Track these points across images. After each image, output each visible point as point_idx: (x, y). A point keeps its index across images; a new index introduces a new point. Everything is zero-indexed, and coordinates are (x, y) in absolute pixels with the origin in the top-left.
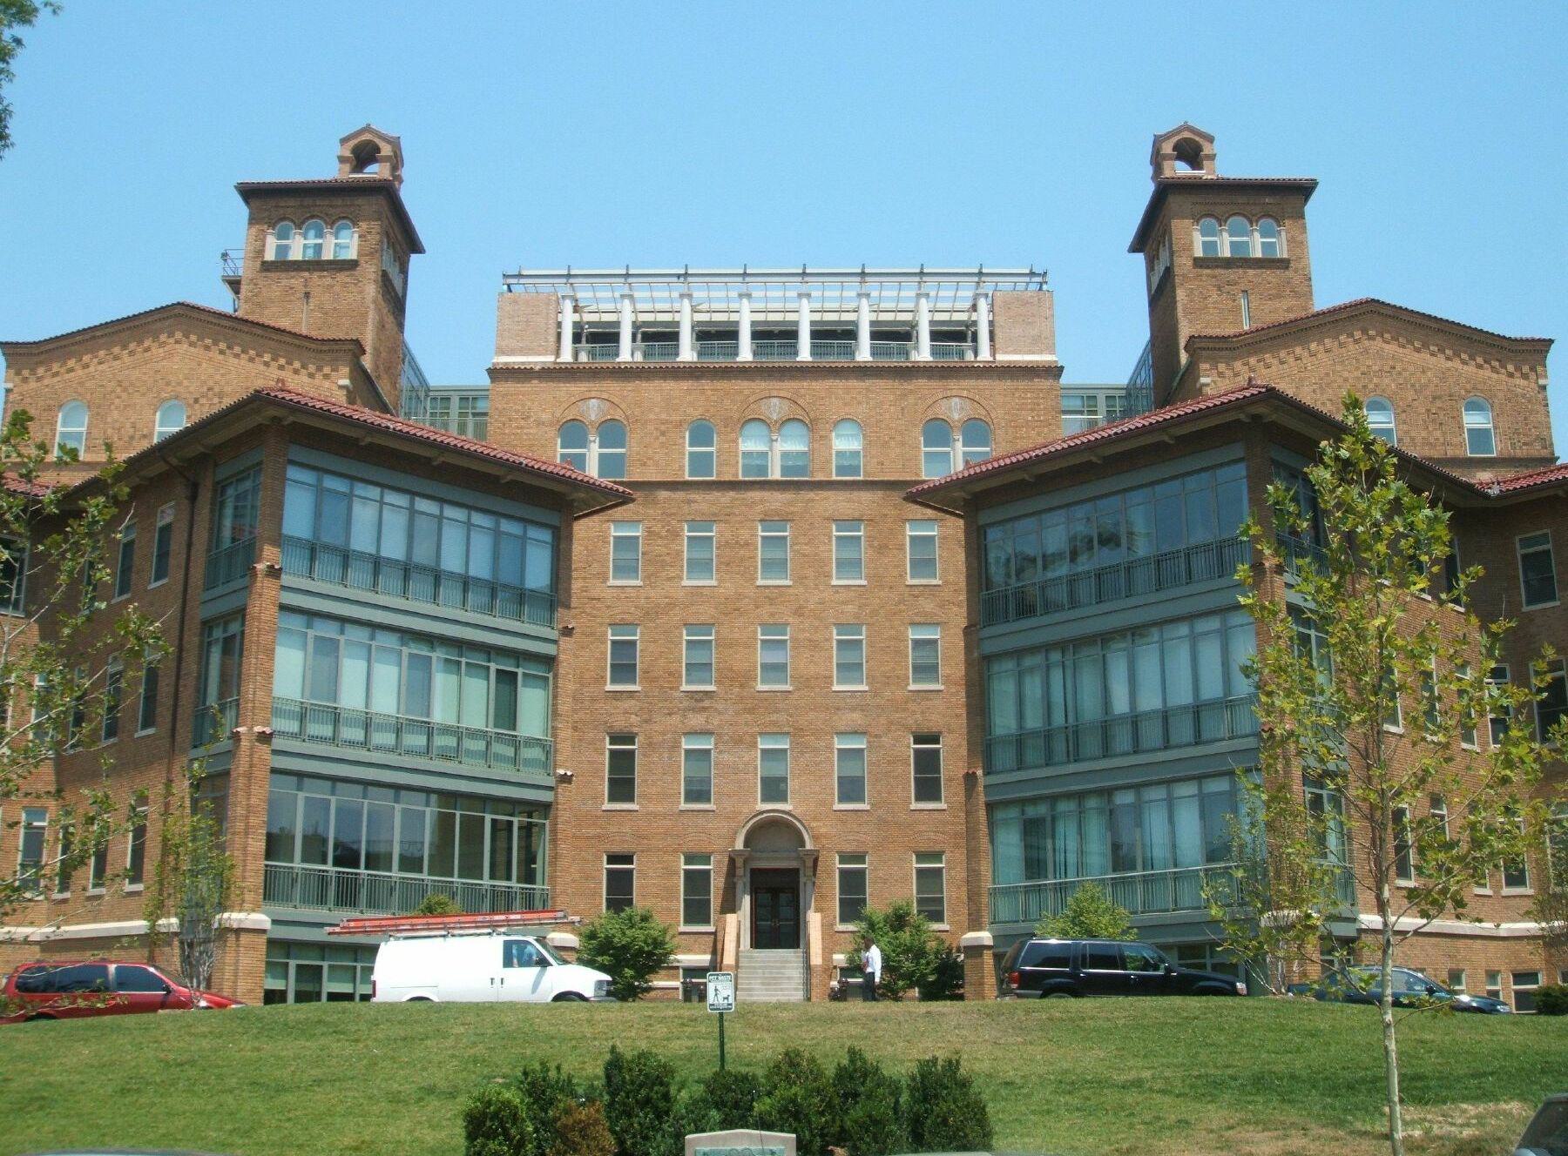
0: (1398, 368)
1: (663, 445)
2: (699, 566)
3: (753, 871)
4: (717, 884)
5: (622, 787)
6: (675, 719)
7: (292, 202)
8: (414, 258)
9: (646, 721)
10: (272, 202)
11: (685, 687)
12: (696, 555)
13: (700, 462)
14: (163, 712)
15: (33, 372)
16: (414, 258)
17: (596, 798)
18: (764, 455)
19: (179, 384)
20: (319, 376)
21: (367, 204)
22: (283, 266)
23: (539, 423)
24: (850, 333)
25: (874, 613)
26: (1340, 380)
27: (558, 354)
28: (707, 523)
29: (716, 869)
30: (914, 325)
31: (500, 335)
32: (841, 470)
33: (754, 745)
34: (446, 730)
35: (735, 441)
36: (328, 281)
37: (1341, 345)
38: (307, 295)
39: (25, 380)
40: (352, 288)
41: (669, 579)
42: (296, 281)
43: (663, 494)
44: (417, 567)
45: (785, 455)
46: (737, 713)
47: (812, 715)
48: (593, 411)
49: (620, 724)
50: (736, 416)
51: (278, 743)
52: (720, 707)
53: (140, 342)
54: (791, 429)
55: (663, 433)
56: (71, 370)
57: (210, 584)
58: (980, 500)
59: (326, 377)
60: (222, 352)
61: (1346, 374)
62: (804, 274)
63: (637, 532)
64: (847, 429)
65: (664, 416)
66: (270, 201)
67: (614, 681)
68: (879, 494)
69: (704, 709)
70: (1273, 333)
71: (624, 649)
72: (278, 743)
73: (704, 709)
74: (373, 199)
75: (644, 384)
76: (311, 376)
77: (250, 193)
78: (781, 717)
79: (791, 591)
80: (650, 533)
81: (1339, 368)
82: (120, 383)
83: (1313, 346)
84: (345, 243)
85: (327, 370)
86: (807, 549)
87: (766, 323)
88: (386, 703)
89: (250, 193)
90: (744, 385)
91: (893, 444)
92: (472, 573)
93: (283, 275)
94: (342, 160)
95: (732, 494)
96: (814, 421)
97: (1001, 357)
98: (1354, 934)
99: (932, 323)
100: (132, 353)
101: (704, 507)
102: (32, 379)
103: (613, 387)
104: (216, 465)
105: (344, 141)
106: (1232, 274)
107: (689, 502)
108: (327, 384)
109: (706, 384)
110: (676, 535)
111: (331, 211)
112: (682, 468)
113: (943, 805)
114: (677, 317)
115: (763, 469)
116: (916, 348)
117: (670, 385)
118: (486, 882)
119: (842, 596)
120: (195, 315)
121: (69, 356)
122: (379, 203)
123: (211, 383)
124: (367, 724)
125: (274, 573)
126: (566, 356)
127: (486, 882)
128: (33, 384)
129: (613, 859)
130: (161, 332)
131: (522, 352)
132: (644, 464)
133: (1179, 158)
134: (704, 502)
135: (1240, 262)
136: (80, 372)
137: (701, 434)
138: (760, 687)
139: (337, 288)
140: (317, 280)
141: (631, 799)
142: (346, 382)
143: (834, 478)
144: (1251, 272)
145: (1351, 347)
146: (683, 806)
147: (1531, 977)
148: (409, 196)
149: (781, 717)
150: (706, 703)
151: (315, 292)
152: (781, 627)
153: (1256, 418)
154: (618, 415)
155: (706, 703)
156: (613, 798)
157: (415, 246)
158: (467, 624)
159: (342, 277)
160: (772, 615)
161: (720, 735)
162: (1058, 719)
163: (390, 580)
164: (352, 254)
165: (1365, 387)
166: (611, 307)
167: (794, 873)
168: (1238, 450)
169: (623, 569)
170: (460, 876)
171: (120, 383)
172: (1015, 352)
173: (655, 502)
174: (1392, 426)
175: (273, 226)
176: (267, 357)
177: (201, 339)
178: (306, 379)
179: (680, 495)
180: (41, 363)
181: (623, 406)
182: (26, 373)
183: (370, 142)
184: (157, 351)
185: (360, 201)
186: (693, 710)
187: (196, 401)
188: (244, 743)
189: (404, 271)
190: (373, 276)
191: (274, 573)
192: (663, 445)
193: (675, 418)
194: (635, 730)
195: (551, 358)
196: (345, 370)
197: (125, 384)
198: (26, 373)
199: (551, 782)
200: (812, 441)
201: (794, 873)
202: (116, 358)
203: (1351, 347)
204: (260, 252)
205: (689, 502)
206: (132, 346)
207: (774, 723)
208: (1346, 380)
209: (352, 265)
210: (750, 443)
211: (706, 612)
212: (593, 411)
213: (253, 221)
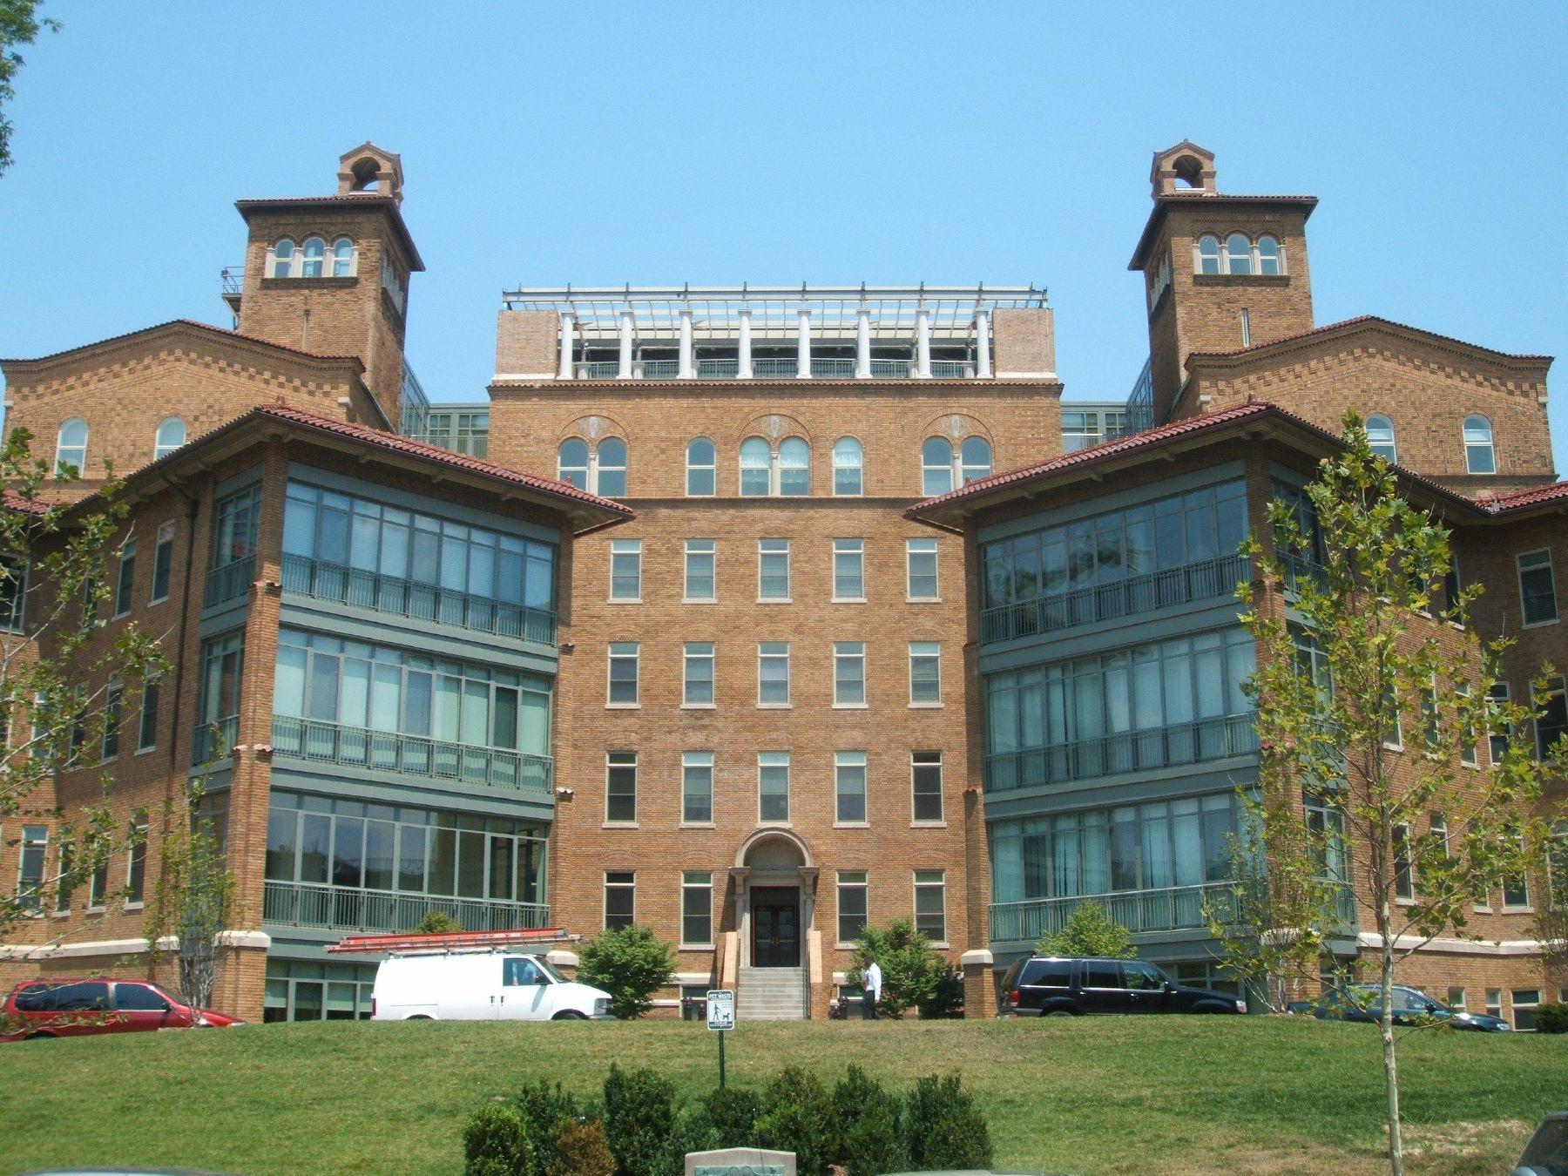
0: (1398, 386)
1: (662, 463)
3: (752, 888)
4: (717, 902)
5: (622, 805)
6: (675, 737)
7: (292, 220)
8: (415, 276)
9: (646, 739)
10: (272, 220)
11: (685, 705)
12: (697, 573)
13: (700, 480)
14: (163, 731)
16: (414, 274)
17: (596, 816)
18: (764, 472)
19: (180, 401)
20: (319, 394)
22: (283, 283)
23: (540, 441)
25: (874, 631)
26: (1340, 398)
27: (558, 372)
28: (707, 541)
29: (716, 887)
31: (501, 352)
34: (446, 748)
35: (735, 459)
36: (329, 298)
37: (1341, 363)
38: (307, 313)
39: (25, 398)
41: (669, 597)
42: (297, 299)
43: (663, 512)
45: (785, 473)
47: (812, 733)
48: (593, 428)
49: (620, 742)
50: (736, 434)
51: (278, 761)
52: (720, 725)
53: (140, 360)
55: (663, 451)
56: (71, 388)
57: (211, 600)
59: (326, 394)
60: (222, 370)
61: (1346, 392)
62: (804, 292)
63: (638, 550)
65: (664, 434)
66: (269, 219)
67: (613, 699)
68: (878, 513)
69: (705, 727)
70: (1273, 351)
71: (624, 667)
72: (278, 761)
73: (705, 727)
74: (373, 217)
75: (645, 402)
76: (311, 393)
77: (250, 210)
78: (781, 735)
79: (791, 609)
80: (650, 551)
81: (1338, 385)
82: (120, 401)
83: (1313, 363)
84: (345, 261)
85: (327, 388)
88: (386, 721)
89: (250, 210)
90: (744, 403)
91: (892, 461)
93: (283, 293)
95: (732, 512)
98: (1353, 952)
99: (932, 340)
101: (704, 525)
103: (613, 405)
104: (216, 483)
106: (1232, 292)
107: (689, 520)
108: (327, 402)
109: (706, 402)
110: (676, 553)
111: (332, 229)
112: (682, 486)
113: (942, 823)
115: (763, 487)
117: (670, 403)
118: (486, 900)
119: (842, 614)
120: (203, 334)
121: (70, 373)
122: (380, 220)
123: (211, 401)
124: (367, 742)
125: (274, 590)
126: (567, 374)
127: (486, 900)
128: (33, 402)
129: (612, 877)
130: (161, 349)
131: (522, 369)
133: (1179, 175)
134: (704, 520)
135: (1240, 279)
136: (80, 390)
137: (701, 452)
138: (761, 705)
139: (337, 306)
141: (631, 817)
142: (346, 400)
144: (1251, 290)
145: (1351, 364)
146: (683, 824)
147: (1531, 995)
148: (409, 213)
150: (706, 721)
152: (781, 645)
153: (1256, 436)
154: (618, 433)
155: (706, 721)
157: (415, 264)
159: (342, 295)
160: (772, 632)
161: (720, 753)
163: (390, 597)
164: (352, 272)
165: (1365, 404)
167: (794, 891)
168: (1238, 468)
169: (623, 587)
171: (120, 401)
172: (1015, 370)
173: (655, 520)
177: (201, 356)
178: (306, 397)
179: (680, 513)
180: (41, 381)
181: (623, 424)
182: (26, 390)
183: (370, 159)
184: (157, 369)
185: (360, 219)
186: (693, 728)
187: (196, 418)
188: (244, 761)
189: (404, 288)
190: (373, 294)
191: (274, 590)
192: (662, 463)
194: (635, 748)
195: (551, 376)
196: (346, 388)
197: (126, 401)
198: (26, 390)
199: (551, 799)
200: (812, 459)
201: (794, 891)
202: (116, 376)
203: (1351, 364)
204: (260, 270)
205: (689, 520)
206: (132, 364)
207: (775, 741)
208: (1346, 398)
209: (351, 283)
210: (750, 461)
211: (706, 630)
212: (593, 428)
213: (253, 238)
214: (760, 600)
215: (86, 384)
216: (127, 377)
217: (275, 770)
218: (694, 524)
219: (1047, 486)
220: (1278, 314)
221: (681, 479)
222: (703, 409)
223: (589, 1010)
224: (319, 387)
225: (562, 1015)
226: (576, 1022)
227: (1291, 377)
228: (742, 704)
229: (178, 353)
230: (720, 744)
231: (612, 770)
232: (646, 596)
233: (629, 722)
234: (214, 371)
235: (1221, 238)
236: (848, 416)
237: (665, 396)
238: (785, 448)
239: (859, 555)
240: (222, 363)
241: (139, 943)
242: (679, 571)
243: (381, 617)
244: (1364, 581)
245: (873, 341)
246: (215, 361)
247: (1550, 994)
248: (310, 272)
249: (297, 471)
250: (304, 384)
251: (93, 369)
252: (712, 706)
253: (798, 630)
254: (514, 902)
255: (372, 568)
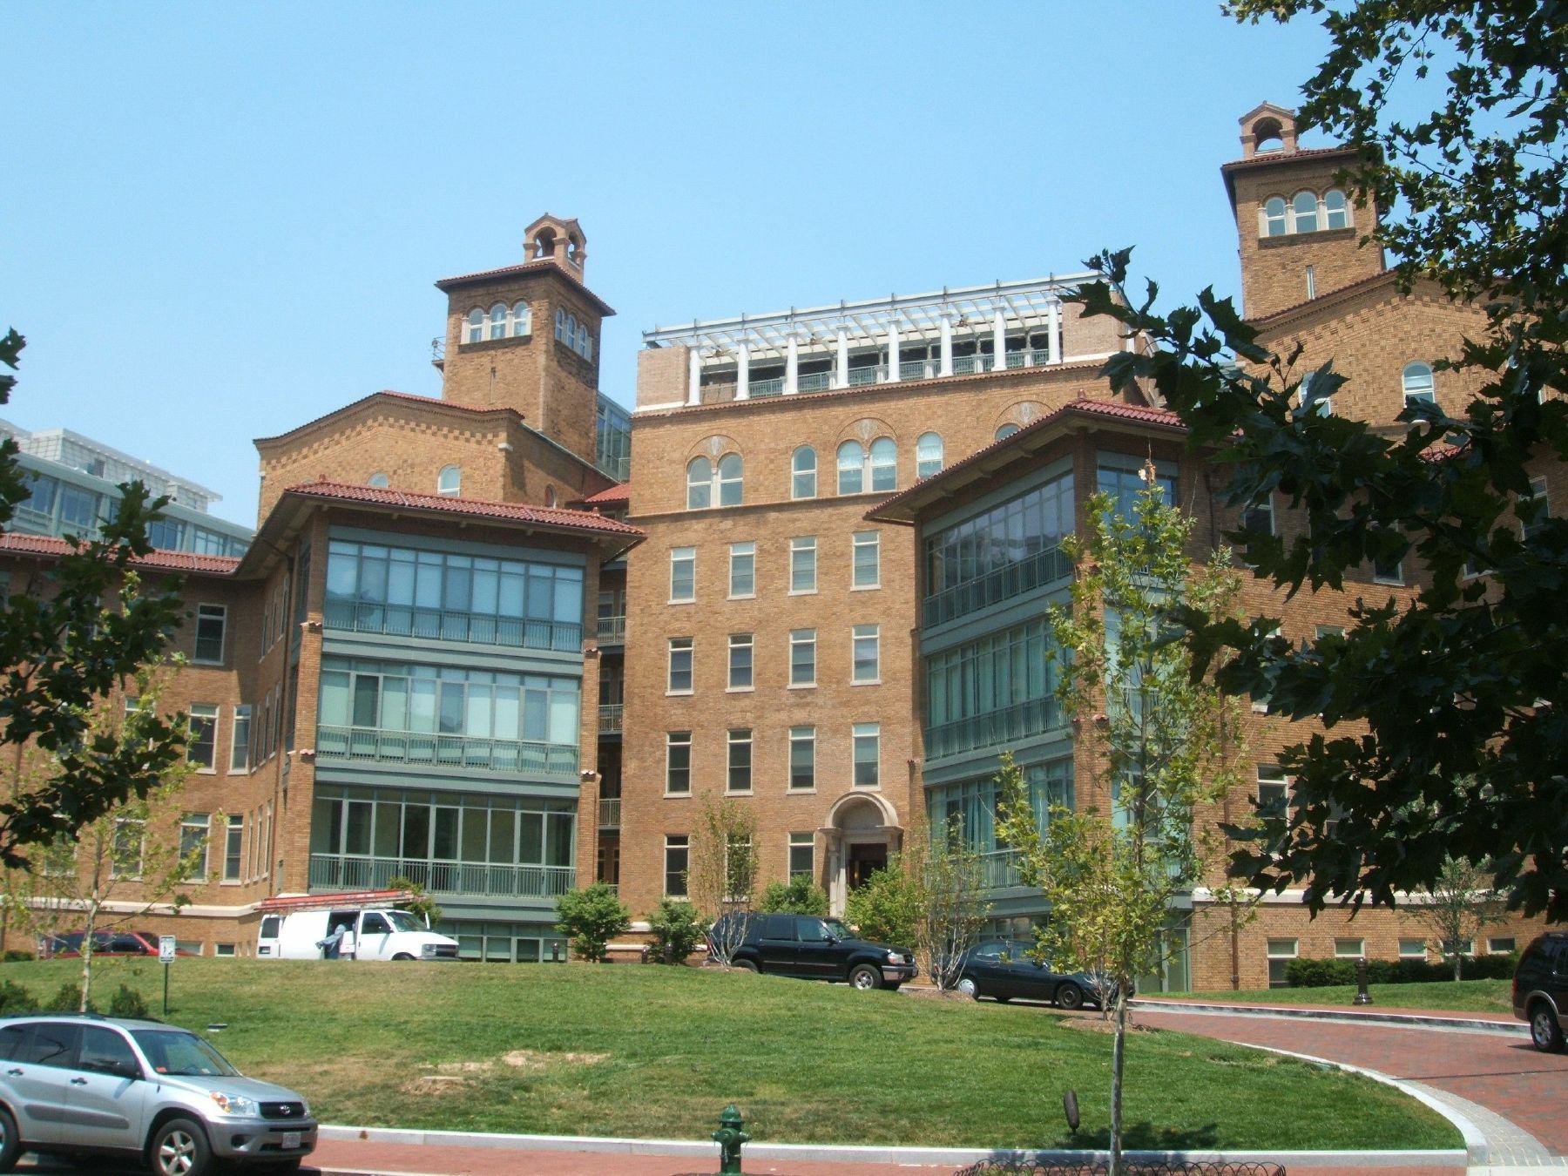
0: (1438, 330)
2: (802, 577)
4: (818, 858)
5: (740, 777)
6: (783, 716)
7: (481, 291)
9: (759, 717)
10: (465, 294)
11: (791, 686)
12: (801, 567)
13: (804, 484)
15: (279, 461)
16: (605, 320)
17: (720, 787)
18: (859, 472)
20: (485, 442)
21: (538, 286)
22: (477, 347)
23: (671, 462)
24: (732, 377)
26: (1377, 349)
27: (687, 400)
28: (809, 537)
29: (817, 845)
30: (784, 360)
31: (640, 388)
32: (844, 488)
33: (849, 734)
34: (479, 743)
35: (833, 463)
37: (1380, 314)
38: (493, 370)
39: (274, 468)
40: (528, 360)
42: (485, 359)
43: (773, 515)
44: (419, 608)
45: (877, 471)
46: (834, 707)
49: (737, 721)
50: (833, 439)
51: (320, 761)
53: (354, 428)
54: (883, 446)
55: (772, 461)
56: (305, 457)
58: (931, 508)
59: (490, 442)
60: (413, 430)
61: (1383, 343)
62: (843, 309)
63: (751, 551)
64: (929, 441)
66: (468, 293)
67: (733, 684)
69: (808, 704)
70: (1306, 310)
71: (741, 656)
72: (320, 761)
73: (808, 704)
74: (543, 281)
75: (756, 418)
76: (479, 443)
77: (448, 287)
78: (872, 709)
80: (761, 550)
81: (1376, 337)
82: (340, 464)
83: (1349, 318)
84: (522, 321)
85: (490, 436)
86: (893, 555)
87: (812, 355)
89: (448, 287)
90: (839, 412)
92: (503, 612)
93: (475, 355)
94: (1244, 140)
95: (830, 510)
96: (899, 437)
97: (1067, 360)
98: (1189, 906)
99: (1007, 331)
100: (348, 438)
101: (805, 524)
102: (1327, 334)
103: (730, 424)
105: (1243, 121)
106: (1297, 250)
107: (794, 521)
108: (490, 449)
109: (809, 414)
110: (784, 550)
111: (511, 295)
112: (787, 491)
114: (1044, 321)
115: (859, 485)
116: (836, 376)
118: (516, 864)
120: (397, 402)
121: (304, 445)
125: (315, 629)
126: (695, 400)
127: (516, 864)
128: (280, 471)
129: (672, 840)
130: (368, 417)
131: (658, 400)
132: (756, 490)
134: (805, 519)
135: (1308, 237)
136: (312, 457)
137: (805, 460)
138: (854, 682)
140: (502, 358)
141: (747, 786)
142: (503, 445)
143: (793, 499)
144: (1316, 246)
145: (1389, 315)
146: (790, 791)
147: (1288, 944)
149: (872, 709)
150: (809, 699)
151: (499, 366)
152: (871, 627)
155: (809, 699)
156: (733, 786)
158: (497, 656)
159: (520, 351)
161: (820, 728)
162: (971, 713)
163: (428, 625)
164: (527, 331)
165: (1403, 353)
166: (881, 331)
167: (882, 848)
169: (741, 584)
170: (492, 860)
171: (340, 464)
172: (1081, 353)
174: (1431, 390)
175: (467, 314)
176: (445, 430)
177: (397, 420)
178: (474, 446)
179: (785, 515)
180: (284, 453)
181: (739, 440)
182: (274, 462)
184: (366, 434)
185: (532, 283)
186: (798, 705)
188: (294, 763)
190: (544, 348)
191: (315, 629)
193: (782, 446)
194: (750, 725)
195: (680, 404)
196: (503, 435)
198: (274, 462)
199: (578, 780)
200: (900, 455)
201: (882, 848)
202: (338, 443)
203: (1389, 315)
204: (458, 337)
205: (794, 521)
206: (348, 432)
207: (866, 714)
208: (1383, 349)
209: (526, 340)
210: (847, 464)
211: (806, 617)
212: (715, 447)
213: (452, 311)
214: (854, 588)
215: (316, 452)
216: (344, 442)
217: (317, 769)
218: (798, 524)
219: (958, 484)
220: (1344, 267)
221: (789, 483)
222: (805, 421)
223: (417, 953)
224: (484, 436)
225: (399, 957)
226: (409, 962)
227: (1327, 334)
228: (838, 682)
229: (381, 418)
230: (820, 719)
231: (732, 746)
232: (760, 590)
233: (745, 703)
234: (407, 432)
235: (1288, 197)
236: (929, 412)
237: (773, 412)
238: (877, 448)
239: (874, 547)
240: (413, 424)
241: (141, 906)
242: (785, 567)
243: (415, 642)
244: (1154, 564)
245: (954, 338)
246: (407, 423)
247: (1482, 944)
248: (498, 336)
249: (335, 531)
250: (473, 435)
251: (320, 439)
252: (813, 685)
253: (886, 613)
254: (543, 866)
255: (408, 602)
